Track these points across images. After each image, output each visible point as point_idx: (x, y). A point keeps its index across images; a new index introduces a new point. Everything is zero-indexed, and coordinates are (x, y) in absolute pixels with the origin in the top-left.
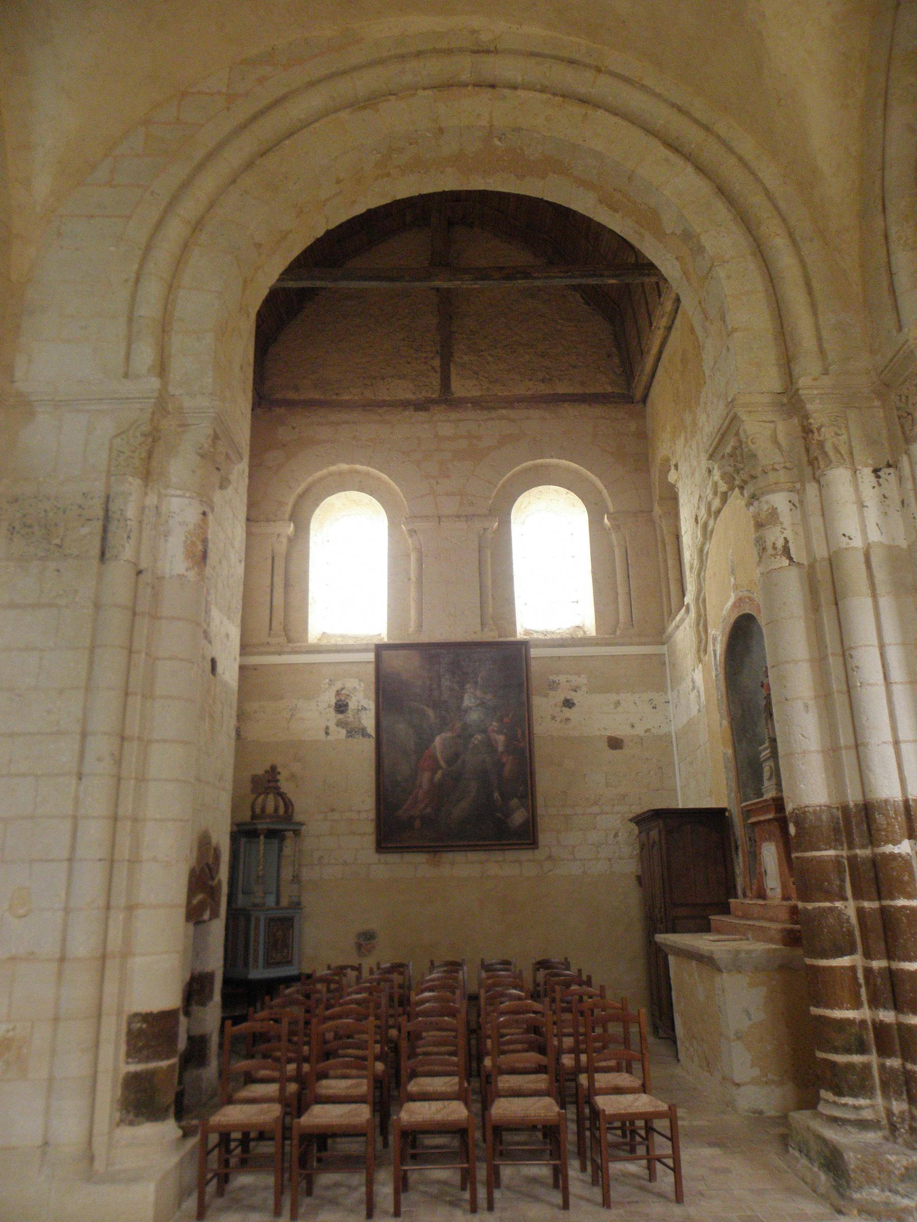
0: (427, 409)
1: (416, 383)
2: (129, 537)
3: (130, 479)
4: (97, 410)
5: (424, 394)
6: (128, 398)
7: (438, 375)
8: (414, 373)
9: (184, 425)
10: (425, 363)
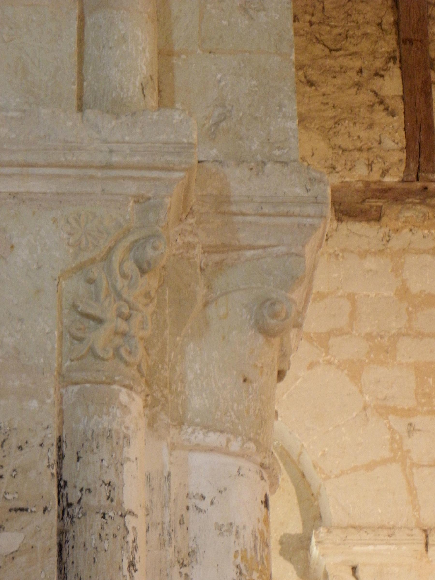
0: (376, 217)
1: (340, 141)
2: (132, 564)
3: (124, 396)
4: (14, 195)
5: (361, 171)
6: (109, 166)
7: (398, 121)
8: (330, 113)
9: (225, 248)
10: (358, 85)
